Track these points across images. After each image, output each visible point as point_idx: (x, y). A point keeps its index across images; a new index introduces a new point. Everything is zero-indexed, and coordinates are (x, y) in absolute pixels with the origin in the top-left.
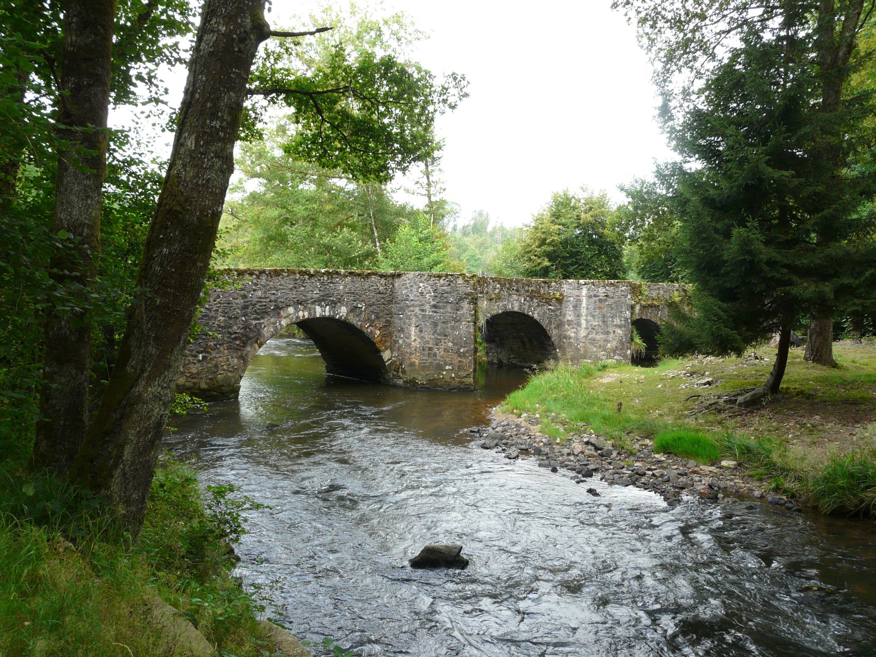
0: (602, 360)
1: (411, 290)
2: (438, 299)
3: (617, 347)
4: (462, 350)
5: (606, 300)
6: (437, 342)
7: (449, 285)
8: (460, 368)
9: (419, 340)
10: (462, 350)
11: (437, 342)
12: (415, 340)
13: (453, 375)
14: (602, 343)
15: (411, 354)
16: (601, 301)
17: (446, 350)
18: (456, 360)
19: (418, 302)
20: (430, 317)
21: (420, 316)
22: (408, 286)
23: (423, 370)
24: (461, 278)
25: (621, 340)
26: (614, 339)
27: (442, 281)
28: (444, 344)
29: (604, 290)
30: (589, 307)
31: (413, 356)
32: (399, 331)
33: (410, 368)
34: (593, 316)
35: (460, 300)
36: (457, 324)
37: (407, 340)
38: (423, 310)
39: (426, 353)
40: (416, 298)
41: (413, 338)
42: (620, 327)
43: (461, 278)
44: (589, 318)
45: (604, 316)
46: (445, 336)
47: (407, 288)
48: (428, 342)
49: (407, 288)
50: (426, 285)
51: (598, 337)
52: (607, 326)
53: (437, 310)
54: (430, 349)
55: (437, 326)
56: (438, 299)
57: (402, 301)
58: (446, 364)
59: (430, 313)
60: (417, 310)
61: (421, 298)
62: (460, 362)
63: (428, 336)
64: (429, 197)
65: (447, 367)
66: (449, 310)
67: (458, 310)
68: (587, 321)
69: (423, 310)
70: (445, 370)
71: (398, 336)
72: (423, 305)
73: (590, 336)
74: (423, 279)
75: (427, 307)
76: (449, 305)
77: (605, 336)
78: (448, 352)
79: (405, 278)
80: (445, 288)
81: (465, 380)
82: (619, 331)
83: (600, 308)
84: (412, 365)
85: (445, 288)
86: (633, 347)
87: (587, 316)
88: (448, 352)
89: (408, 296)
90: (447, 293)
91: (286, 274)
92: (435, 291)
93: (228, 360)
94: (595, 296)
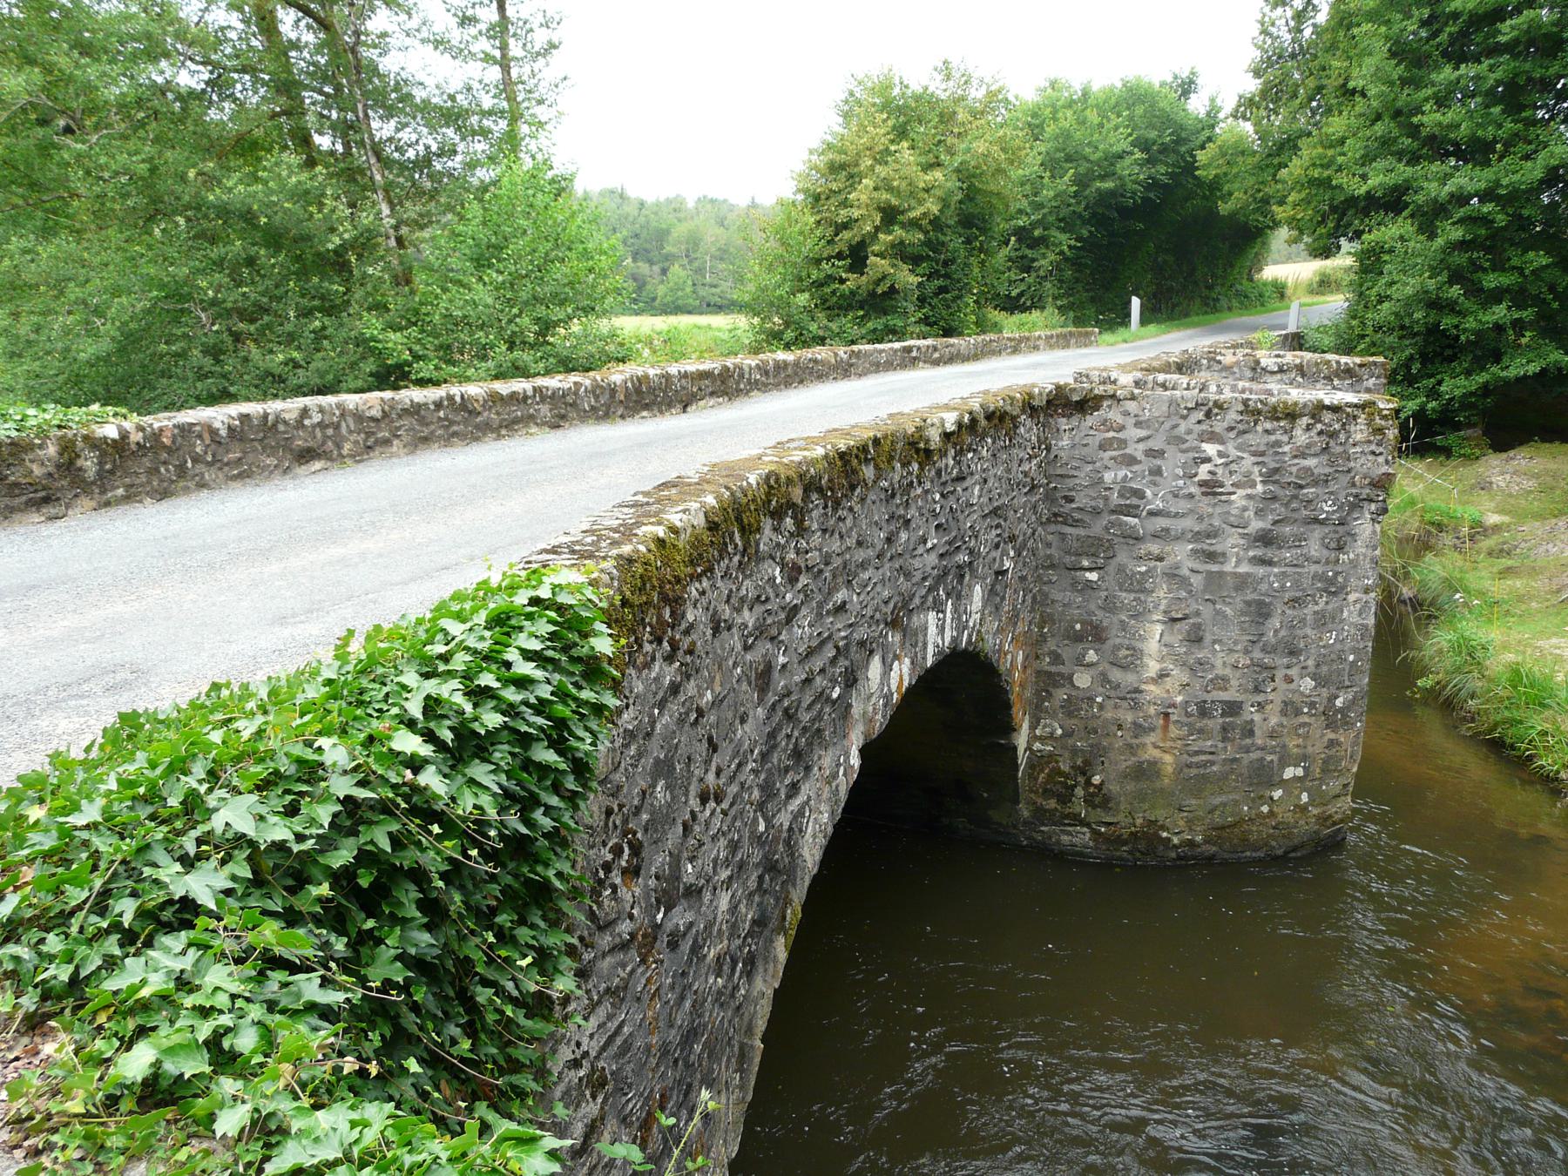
1: (1157, 472)
4: (1339, 703)
6: (1260, 678)
7: (1325, 449)
10: (1339, 703)
12: (1163, 675)
13: (1305, 797)
15: (1139, 729)
17: (1290, 709)
19: (1188, 523)
20: (1242, 582)
21: (1197, 581)
22: (1137, 450)
27: (1301, 437)
32: (1078, 638)
33: (1131, 786)
37: (1116, 675)
38: (1211, 556)
39: (1215, 723)
40: (1182, 506)
41: (1153, 667)
46: (1293, 652)
47: (1131, 461)
48: (1222, 682)
49: (1131, 461)
50: (1234, 453)
53: (1270, 553)
54: (1233, 708)
55: (1267, 616)
57: (1096, 512)
58: (1285, 762)
59: (1244, 568)
60: (1181, 554)
61: (1205, 505)
62: (1332, 743)
64: (506, 69)
65: (1289, 773)
67: (1340, 548)
69: (1211, 556)
70: (1283, 783)
71: (1067, 653)
72: (1212, 534)
74: (1219, 426)
75: (1231, 543)
76: (1317, 532)
78: (1298, 713)
79: (1114, 415)
80: (1311, 462)
84: (1143, 772)
85: (1311, 462)
88: (1298, 713)
89: (1139, 494)
90: (1315, 483)
92: (1270, 476)
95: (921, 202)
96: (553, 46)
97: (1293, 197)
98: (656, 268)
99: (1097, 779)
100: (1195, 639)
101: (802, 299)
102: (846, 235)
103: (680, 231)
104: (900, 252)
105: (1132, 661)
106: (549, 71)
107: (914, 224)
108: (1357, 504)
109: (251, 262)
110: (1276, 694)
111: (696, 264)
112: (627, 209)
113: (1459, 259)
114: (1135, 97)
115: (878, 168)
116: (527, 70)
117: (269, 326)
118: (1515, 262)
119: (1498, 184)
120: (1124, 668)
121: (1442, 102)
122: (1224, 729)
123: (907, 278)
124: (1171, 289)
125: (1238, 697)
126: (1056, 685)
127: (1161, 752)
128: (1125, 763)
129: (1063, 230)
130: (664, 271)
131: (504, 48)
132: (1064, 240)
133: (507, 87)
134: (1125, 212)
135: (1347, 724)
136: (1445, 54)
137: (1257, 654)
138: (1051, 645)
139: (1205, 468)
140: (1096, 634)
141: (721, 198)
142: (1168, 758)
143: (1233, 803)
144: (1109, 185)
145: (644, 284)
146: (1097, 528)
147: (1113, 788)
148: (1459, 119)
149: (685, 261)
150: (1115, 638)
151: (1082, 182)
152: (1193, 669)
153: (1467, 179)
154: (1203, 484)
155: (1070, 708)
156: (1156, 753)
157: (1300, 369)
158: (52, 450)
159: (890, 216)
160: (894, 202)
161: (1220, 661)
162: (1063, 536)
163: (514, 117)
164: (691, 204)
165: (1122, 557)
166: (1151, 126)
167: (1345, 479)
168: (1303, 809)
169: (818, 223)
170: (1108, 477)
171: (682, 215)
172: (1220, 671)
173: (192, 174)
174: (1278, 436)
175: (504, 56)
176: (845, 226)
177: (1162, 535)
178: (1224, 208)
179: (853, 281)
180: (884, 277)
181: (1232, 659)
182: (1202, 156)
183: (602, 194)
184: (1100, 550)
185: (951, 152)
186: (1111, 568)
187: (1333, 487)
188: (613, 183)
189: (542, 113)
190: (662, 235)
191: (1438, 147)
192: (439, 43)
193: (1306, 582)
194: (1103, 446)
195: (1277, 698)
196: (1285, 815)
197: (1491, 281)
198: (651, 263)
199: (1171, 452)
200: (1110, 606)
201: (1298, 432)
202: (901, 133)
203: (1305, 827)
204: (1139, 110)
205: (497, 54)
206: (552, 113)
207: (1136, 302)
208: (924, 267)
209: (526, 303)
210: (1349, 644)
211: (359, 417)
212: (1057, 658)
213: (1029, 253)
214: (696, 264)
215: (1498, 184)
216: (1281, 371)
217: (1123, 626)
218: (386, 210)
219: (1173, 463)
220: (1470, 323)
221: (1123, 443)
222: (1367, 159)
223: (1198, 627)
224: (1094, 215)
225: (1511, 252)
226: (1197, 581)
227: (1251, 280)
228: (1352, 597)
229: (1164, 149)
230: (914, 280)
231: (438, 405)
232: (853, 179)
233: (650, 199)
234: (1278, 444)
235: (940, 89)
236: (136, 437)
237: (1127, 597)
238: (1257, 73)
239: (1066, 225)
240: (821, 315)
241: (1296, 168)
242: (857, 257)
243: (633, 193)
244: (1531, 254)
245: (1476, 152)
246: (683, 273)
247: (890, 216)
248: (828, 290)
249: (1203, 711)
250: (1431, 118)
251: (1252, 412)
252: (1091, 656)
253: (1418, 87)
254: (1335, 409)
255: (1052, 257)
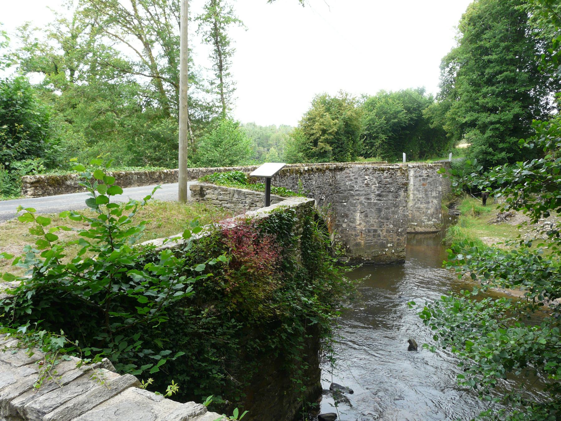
0: (424, 222)
1: (357, 182)
2: (382, 189)
3: (434, 213)
4: (399, 230)
5: (427, 179)
6: (381, 225)
7: (391, 177)
8: (399, 245)
9: (364, 224)
10: (399, 230)
11: (381, 225)
12: (360, 224)
13: (393, 251)
14: (424, 210)
15: (356, 236)
16: (424, 179)
17: (388, 231)
18: (395, 238)
19: (363, 192)
20: (375, 204)
21: (366, 204)
22: (353, 178)
23: (369, 249)
24: (399, 171)
25: (436, 208)
26: (432, 207)
27: (385, 174)
28: (386, 226)
29: (426, 172)
30: (416, 184)
31: (359, 237)
32: (343, 217)
33: (355, 248)
34: (419, 191)
35: (399, 189)
36: (396, 209)
37: (351, 224)
38: (368, 199)
39: (372, 234)
40: (362, 189)
41: (358, 222)
42: (435, 198)
43: (399, 171)
44: (415, 192)
45: (426, 191)
46: (388, 219)
47: (351, 180)
48: (373, 225)
49: (351, 180)
50: (371, 178)
51: (422, 206)
52: (428, 198)
53: (380, 198)
54: (375, 231)
55: (381, 211)
56: (382, 189)
57: (345, 191)
58: (388, 243)
59: (375, 201)
60: (362, 199)
61: (366, 189)
62: (398, 239)
63: (373, 220)
64: (222, 95)
65: (389, 245)
66: (390, 198)
67: (397, 198)
68: (413, 194)
69: (368, 199)
70: (387, 247)
71: (341, 220)
72: (368, 194)
73: (416, 206)
74: (368, 172)
75: (372, 196)
76: (391, 194)
77: (426, 205)
78: (390, 232)
79: (348, 171)
80: (388, 180)
81: (400, 254)
82: (435, 201)
83: (423, 185)
84: (358, 245)
85: (388, 180)
86: (443, 212)
87: (413, 190)
88: (390, 232)
89: (353, 187)
90: (389, 184)
91: (288, 174)
92: (379, 183)
93: (472, 297)
94: (420, 176)
95: (332, 128)
96: (234, 89)
97: (448, 123)
98: (266, 149)
99: (348, 247)
100: (366, 216)
101: (301, 154)
102: (313, 137)
103: (273, 136)
104: (327, 141)
105: (354, 221)
106: (234, 95)
107: (330, 134)
108: (400, 188)
109: (158, 146)
110: (385, 228)
111: (279, 147)
112: (256, 129)
113: (492, 140)
114: (404, 97)
115: (321, 119)
116: (228, 95)
117: (162, 162)
118: (508, 140)
119: (501, 119)
120: (352, 223)
121: (484, 97)
122: (374, 235)
123: (329, 148)
124: (425, 151)
125: (376, 228)
126: (339, 227)
127: (361, 241)
128: (354, 243)
129: (383, 134)
130: (268, 150)
131: (222, 90)
132: (384, 137)
133: (222, 100)
134: (404, 129)
135: (402, 235)
136: (485, 83)
137: (380, 219)
138: (338, 218)
139: (366, 181)
140: (346, 216)
141: (288, 125)
142: (362, 242)
143: (378, 251)
144: (396, 120)
145: (262, 154)
146: (346, 194)
147: (351, 248)
148: (489, 101)
149: (276, 146)
150: (350, 216)
151: (388, 120)
152: (367, 222)
153: (493, 118)
154: (366, 184)
155: (342, 232)
156: (360, 241)
157: (418, 167)
158: (158, 173)
159: (324, 132)
160: (325, 128)
161: (372, 221)
162: (339, 196)
163: (224, 108)
164: (278, 128)
165: (351, 200)
166: (410, 103)
167: (396, 183)
168: (393, 253)
169: (305, 134)
170: (347, 183)
171: (274, 131)
172: (372, 223)
173: (145, 125)
174: (381, 174)
175: (222, 92)
176: (313, 135)
177: (358, 195)
178: (431, 126)
179: (314, 149)
180: (323, 148)
181: (374, 220)
182: (424, 112)
183: (248, 125)
184: (346, 198)
185: (341, 115)
186: (349, 202)
187: (393, 185)
188: (251, 121)
189: (231, 106)
190: (267, 138)
191: (485, 109)
192: (208, 92)
193: (389, 204)
194: (346, 178)
195: (385, 229)
196: (389, 254)
197: (501, 146)
198: (264, 147)
199: (359, 178)
200: (349, 210)
201: (385, 174)
202: (328, 110)
203: (394, 258)
204: (406, 98)
205: (220, 92)
206: (234, 106)
207: (404, 154)
208: (334, 145)
209: (227, 156)
210: (401, 218)
211: (202, 172)
212: (339, 221)
213: (372, 141)
214: (279, 147)
215: (501, 119)
216: (413, 167)
217: (352, 214)
218: (191, 132)
219: (360, 180)
220: (496, 158)
221: (350, 177)
222: (467, 112)
223: (366, 213)
224: (393, 129)
225: (507, 137)
226: (366, 204)
227: (454, 148)
228: (400, 208)
229: (415, 109)
230: (331, 148)
231: (215, 170)
232: (314, 122)
233: (264, 126)
234: (380, 176)
235: (339, 97)
236: (169, 172)
237: (352, 208)
238: (441, 87)
239: (384, 132)
240: (306, 158)
241: (448, 114)
242: (315, 143)
243: (258, 124)
244: (512, 138)
245: (493, 110)
246: (274, 150)
247: (324, 132)
248: (308, 152)
249: (369, 232)
250: (481, 101)
251: (375, 170)
252: (346, 220)
253: (478, 92)
254: (393, 169)
255: (380, 142)
